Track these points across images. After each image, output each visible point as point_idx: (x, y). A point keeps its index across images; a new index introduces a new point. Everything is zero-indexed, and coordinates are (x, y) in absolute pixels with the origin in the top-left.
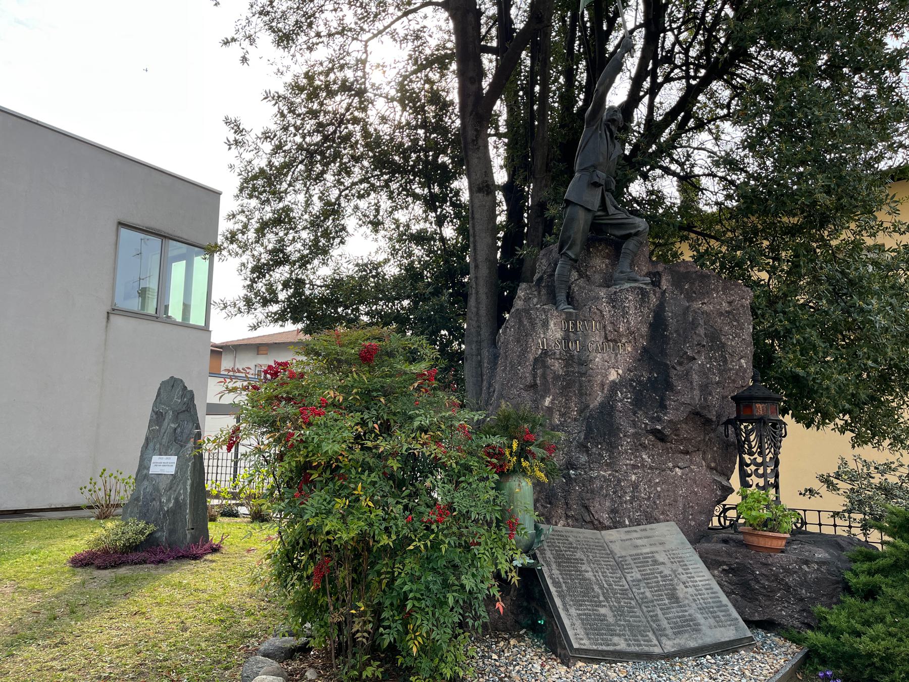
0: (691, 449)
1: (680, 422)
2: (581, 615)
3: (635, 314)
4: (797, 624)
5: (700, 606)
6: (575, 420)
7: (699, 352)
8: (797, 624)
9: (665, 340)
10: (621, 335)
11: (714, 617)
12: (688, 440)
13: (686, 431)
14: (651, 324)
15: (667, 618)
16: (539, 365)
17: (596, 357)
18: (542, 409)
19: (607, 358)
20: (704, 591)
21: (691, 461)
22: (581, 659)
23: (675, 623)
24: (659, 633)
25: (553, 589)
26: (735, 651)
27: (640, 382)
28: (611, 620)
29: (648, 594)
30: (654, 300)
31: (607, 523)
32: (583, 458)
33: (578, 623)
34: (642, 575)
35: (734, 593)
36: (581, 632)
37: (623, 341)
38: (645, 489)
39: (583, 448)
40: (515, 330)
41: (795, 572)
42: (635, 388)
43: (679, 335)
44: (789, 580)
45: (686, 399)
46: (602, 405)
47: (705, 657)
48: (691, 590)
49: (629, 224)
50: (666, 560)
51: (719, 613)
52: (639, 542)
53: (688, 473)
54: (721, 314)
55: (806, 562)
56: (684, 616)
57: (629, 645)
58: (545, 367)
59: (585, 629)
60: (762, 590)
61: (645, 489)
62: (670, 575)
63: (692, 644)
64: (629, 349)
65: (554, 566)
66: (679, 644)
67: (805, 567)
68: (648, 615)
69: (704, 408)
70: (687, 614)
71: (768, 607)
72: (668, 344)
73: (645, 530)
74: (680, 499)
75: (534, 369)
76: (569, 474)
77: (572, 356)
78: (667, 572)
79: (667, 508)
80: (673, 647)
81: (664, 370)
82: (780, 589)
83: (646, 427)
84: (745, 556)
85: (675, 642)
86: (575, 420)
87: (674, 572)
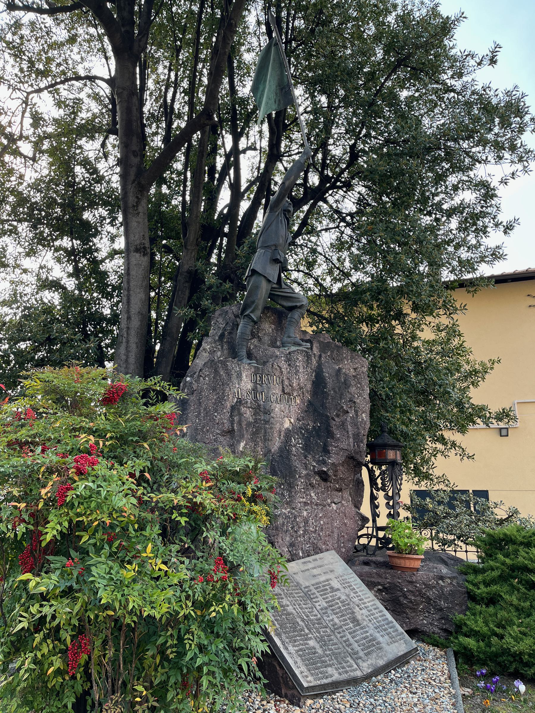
4: (436, 630)
8: (436, 630)
9: (325, 395)
14: (313, 382)
15: (356, 641)
16: (236, 413)
22: (308, 697)
23: (364, 645)
27: (307, 430)
28: (320, 651)
29: (336, 620)
33: (299, 660)
34: (327, 602)
36: (303, 668)
40: (210, 379)
41: (434, 587)
42: (304, 435)
43: (335, 392)
44: (430, 594)
45: (343, 445)
46: (280, 448)
50: (339, 586)
52: (315, 572)
56: (367, 637)
57: (340, 674)
58: (240, 415)
63: (381, 663)
64: (298, 401)
66: (372, 664)
67: (440, 582)
74: (335, 530)
75: (231, 416)
77: (259, 406)
78: (343, 597)
79: (327, 539)
82: (422, 602)
84: (393, 576)
87: (348, 596)
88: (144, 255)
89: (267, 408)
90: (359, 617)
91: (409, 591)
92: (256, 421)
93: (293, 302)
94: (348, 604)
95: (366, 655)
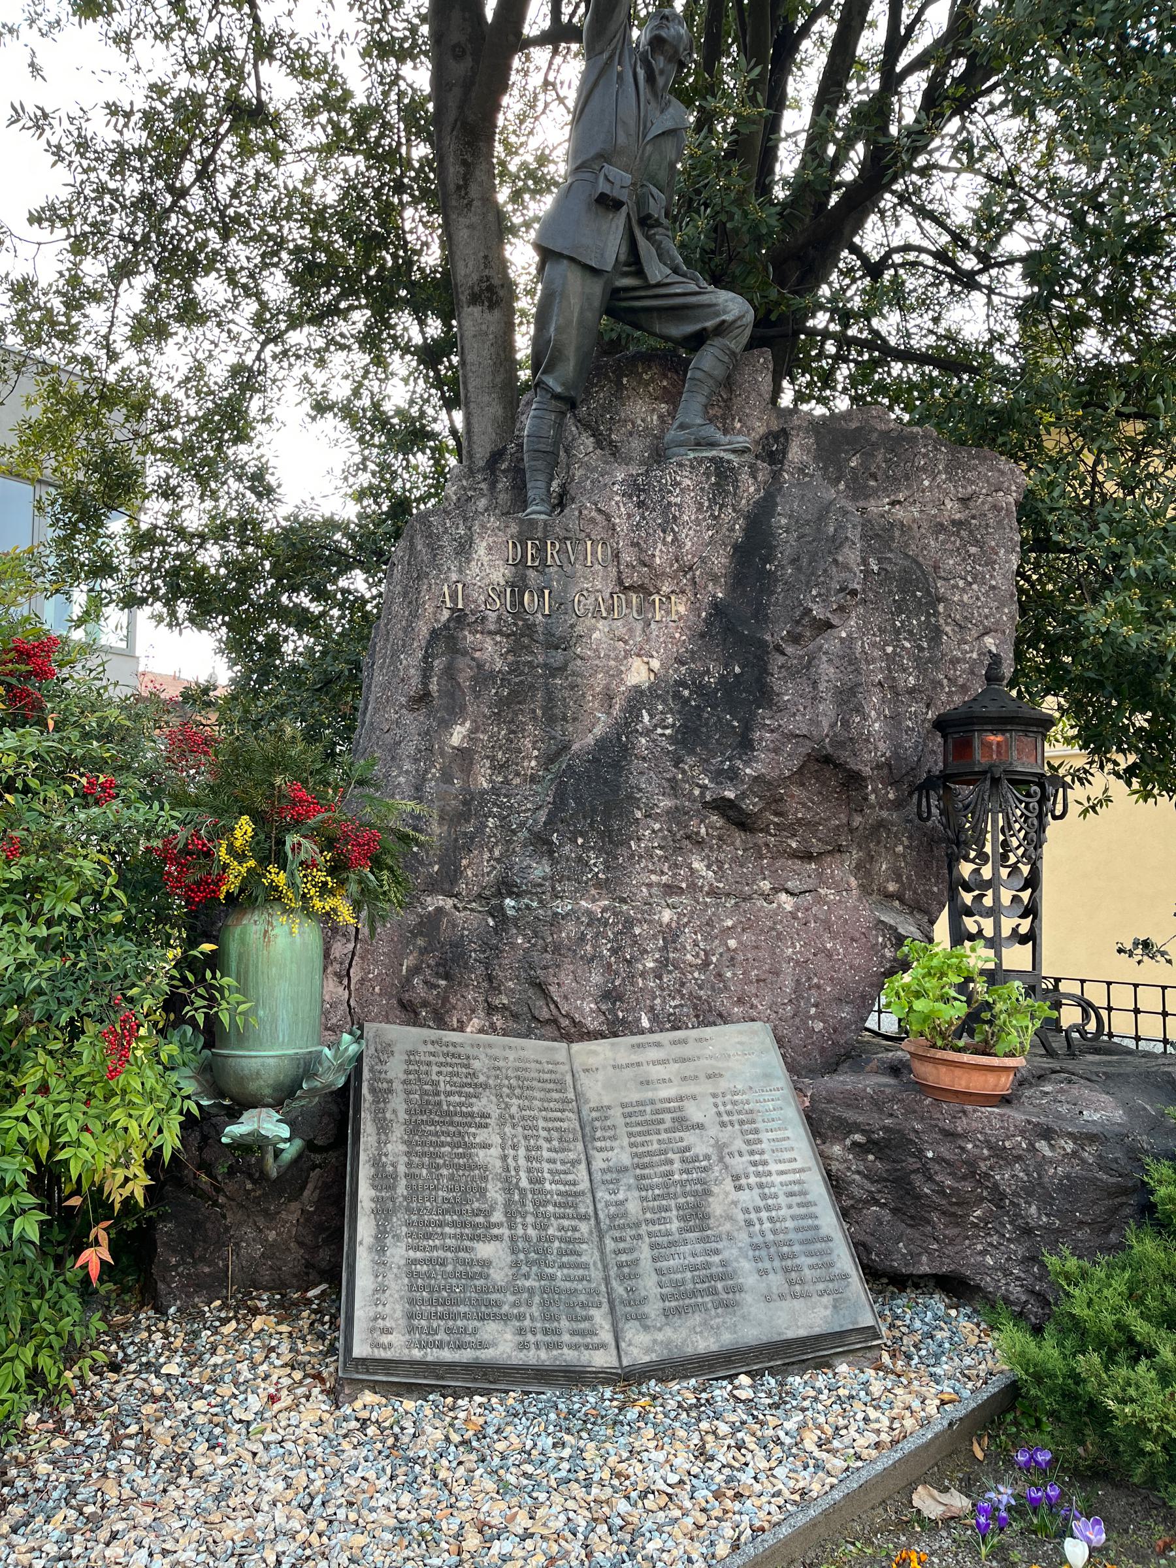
0: (816, 847)
1: (784, 781)
2: (415, 1262)
3: (697, 522)
5: (758, 1240)
6: (533, 779)
7: (841, 609)
8: (1016, 1292)
9: (766, 582)
10: (658, 575)
11: (786, 1270)
12: (811, 825)
13: (801, 802)
14: (736, 547)
15: (659, 1272)
17: (594, 629)
18: (442, 753)
19: (620, 628)
20: (782, 1200)
21: (820, 875)
22: (374, 1387)
23: (676, 1284)
24: (627, 1309)
25: (365, 1193)
26: (824, 1364)
29: (633, 1207)
30: (750, 489)
31: (592, 1023)
32: (540, 869)
33: (397, 1286)
35: (876, 1202)
36: (395, 1310)
37: (666, 589)
38: (696, 944)
39: (541, 844)
41: (1019, 1158)
42: (686, 701)
43: (799, 569)
45: (797, 724)
46: (602, 744)
47: (731, 1378)
48: (748, 1198)
49: (710, 306)
51: (803, 1260)
53: (817, 908)
54: (940, 528)
55: (1047, 1134)
59: (412, 1302)
60: (936, 1199)
61: (696, 944)
62: (707, 1157)
63: (704, 1344)
64: (682, 609)
65: (398, 1132)
67: (1042, 1145)
68: (612, 1259)
69: (841, 745)
70: (716, 1259)
71: (952, 1242)
72: (773, 592)
73: (685, 1042)
74: (787, 968)
76: (501, 908)
77: (530, 628)
80: (648, 1351)
81: (757, 657)
83: (702, 794)
84: (909, 1111)
85: (660, 1336)
86: (533, 779)
88: (491, 308)
89: (559, 632)
90: (715, 1207)
91: (939, 1159)
92: (515, 669)
93: (698, 320)
94: (705, 1169)
95: (666, 1313)
